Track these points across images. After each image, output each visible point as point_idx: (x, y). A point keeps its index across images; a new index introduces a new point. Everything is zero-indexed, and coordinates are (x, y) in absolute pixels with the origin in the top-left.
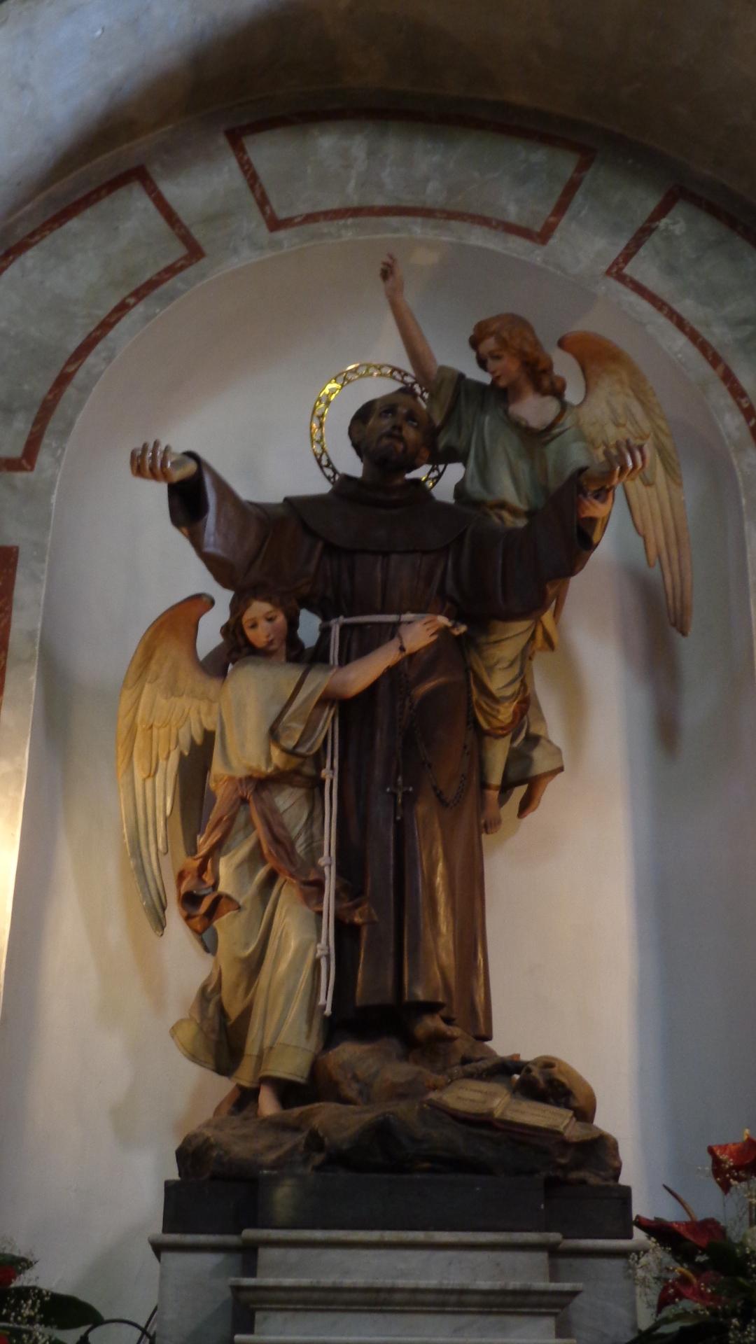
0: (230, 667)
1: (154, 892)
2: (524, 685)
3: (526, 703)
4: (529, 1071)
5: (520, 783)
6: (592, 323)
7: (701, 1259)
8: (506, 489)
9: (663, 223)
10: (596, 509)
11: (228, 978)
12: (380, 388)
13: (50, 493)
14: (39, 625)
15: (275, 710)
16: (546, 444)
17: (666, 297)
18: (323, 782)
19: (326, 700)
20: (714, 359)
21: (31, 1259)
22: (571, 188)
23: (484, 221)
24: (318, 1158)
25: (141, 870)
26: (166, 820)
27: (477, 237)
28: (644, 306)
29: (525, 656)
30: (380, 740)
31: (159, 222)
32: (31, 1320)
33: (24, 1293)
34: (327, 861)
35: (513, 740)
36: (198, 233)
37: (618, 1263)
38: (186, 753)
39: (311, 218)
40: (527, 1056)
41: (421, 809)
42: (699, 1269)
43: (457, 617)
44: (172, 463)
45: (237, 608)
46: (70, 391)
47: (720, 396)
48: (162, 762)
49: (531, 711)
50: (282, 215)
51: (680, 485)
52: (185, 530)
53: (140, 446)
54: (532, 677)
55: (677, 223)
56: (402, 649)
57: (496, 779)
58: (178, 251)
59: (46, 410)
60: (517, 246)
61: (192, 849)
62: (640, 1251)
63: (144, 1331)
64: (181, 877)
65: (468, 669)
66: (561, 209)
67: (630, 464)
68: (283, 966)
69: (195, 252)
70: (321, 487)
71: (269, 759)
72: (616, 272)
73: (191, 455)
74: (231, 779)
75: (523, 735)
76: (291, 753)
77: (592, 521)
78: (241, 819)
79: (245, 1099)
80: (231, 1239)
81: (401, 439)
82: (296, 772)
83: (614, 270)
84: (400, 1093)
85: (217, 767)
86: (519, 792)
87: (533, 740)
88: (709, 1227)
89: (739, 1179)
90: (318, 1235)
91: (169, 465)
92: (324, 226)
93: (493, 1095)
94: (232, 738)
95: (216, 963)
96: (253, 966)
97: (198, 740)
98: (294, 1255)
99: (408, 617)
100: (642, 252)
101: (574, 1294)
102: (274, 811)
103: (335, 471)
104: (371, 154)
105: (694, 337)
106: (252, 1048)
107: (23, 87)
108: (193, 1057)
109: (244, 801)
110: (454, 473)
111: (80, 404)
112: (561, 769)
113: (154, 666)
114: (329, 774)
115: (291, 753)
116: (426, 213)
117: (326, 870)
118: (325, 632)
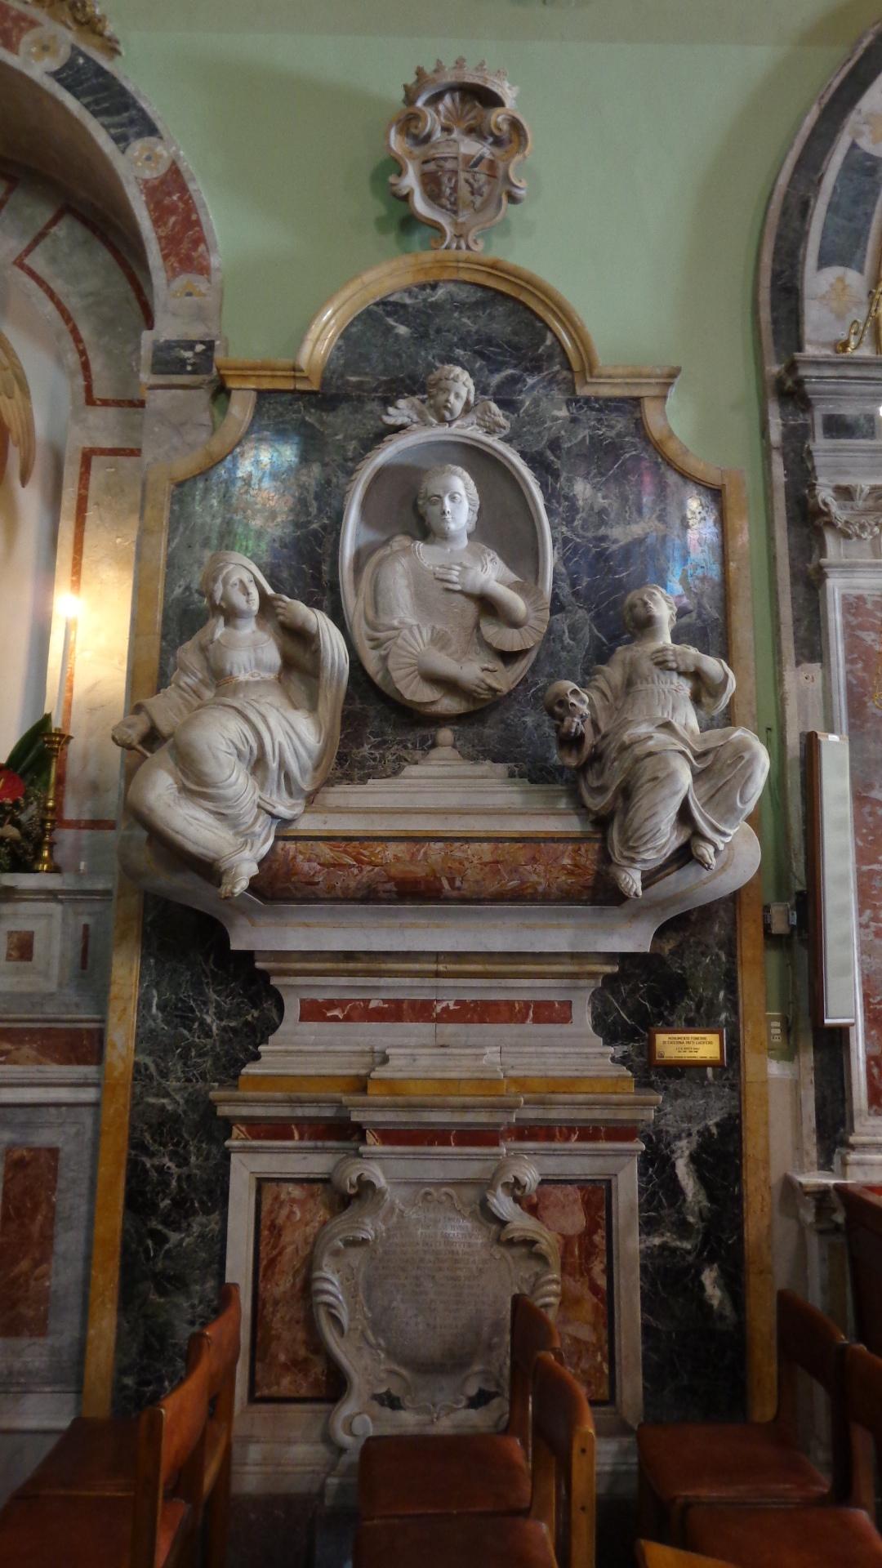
9: (54, 230)
28: (32, 284)
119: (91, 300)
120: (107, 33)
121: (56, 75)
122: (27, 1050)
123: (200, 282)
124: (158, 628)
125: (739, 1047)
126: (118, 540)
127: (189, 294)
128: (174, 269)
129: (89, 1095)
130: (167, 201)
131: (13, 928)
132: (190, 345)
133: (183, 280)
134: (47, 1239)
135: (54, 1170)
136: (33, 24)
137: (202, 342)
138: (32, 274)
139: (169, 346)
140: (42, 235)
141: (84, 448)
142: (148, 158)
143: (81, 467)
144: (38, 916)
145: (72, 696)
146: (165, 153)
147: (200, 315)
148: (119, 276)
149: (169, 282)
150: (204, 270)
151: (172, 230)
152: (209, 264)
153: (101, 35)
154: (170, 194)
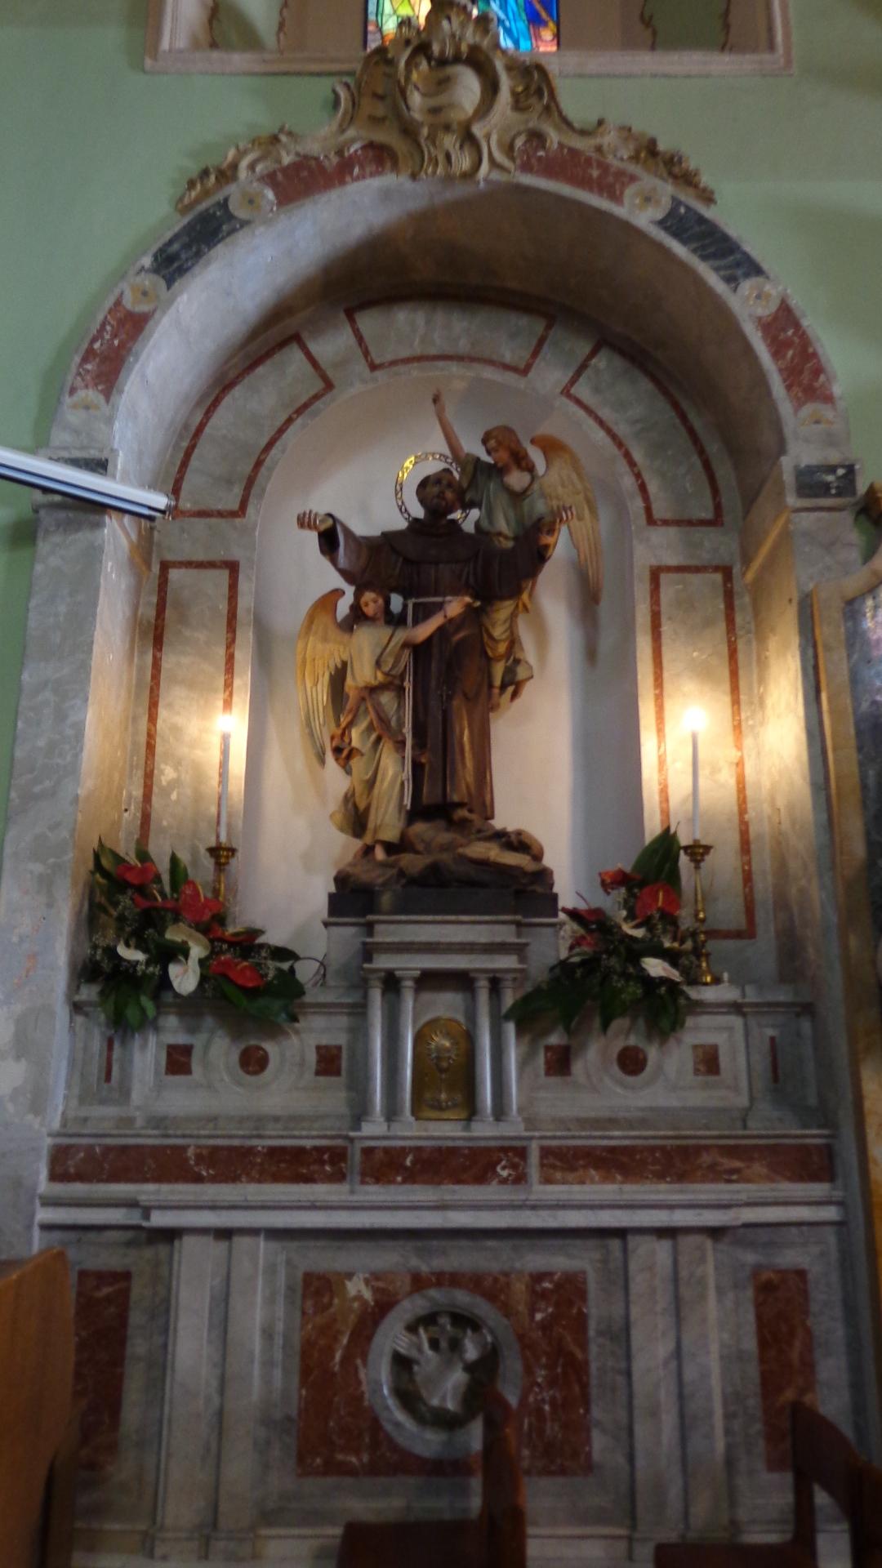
0: (355, 627)
1: (318, 745)
2: (512, 633)
3: (513, 642)
4: (509, 837)
5: (511, 684)
6: (546, 429)
7: (594, 926)
8: (502, 524)
9: (594, 361)
10: (547, 540)
11: (359, 790)
12: (433, 467)
13: (254, 529)
14: (252, 605)
15: (379, 651)
16: (524, 499)
17: (593, 407)
18: (404, 689)
19: (405, 645)
20: (620, 444)
21: (264, 930)
22: (541, 342)
23: (491, 362)
24: (403, 881)
25: (311, 734)
26: (324, 708)
27: (489, 373)
28: (581, 413)
29: (513, 617)
30: (434, 666)
31: (308, 367)
32: (265, 958)
33: (262, 946)
34: (408, 730)
35: (507, 661)
36: (330, 373)
37: (549, 930)
38: (333, 673)
39: (393, 363)
40: (510, 828)
41: (457, 703)
42: (590, 931)
43: (476, 597)
44: (320, 521)
45: (358, 595)
46: (263, 470)
47: (622, 466)
48: (320, 679)
49: (516, 645)
50: (377, 361)
51: (598, 520)
52: (328, 557)
53: (302, 512)
54: (517, 626)
55: (601, 362)
56: (445, 616)
57: (497, 682)
58: (319, 385)
59: (250, 482)
60: (510, 378)
61: (338, 725)
62: (562, 924)
63: (322, 963)
64: (332, 738)
65: (481, 625)
66: (535, 353)
67: (565, 518)
68: (386, 784)
69: (329, 385)
70: (401, 524)
71: (376, 678)
72: (566, 392)
73: (330, 515)
74: (357, 688)
75: (512, 658)
76: (387, 674)
77: (547, 547)
78: (362, 708)
79: (368, 850)
80: (361, 920)
81: (444, 498)
82: (391, 683)
83: (565, 391)
84: (444, 848)
85: (349, 682)
86: (511, 689)
87: (517, 662)
88: (598, 912)
89: (613, 889)
90: (403, 918)
91: (318, 522)
92: (402, 368)
93: (489, 849)
94: (356, 666)
95: (352, 783)
96: (371, 784)
97: (339, 666)
98: (392, 927)
99: (448, 598)
100: (581, 379)
101: (526, 945)
102: (379, 704)
103: (409, 515)
104: (428, 322)
105: (609, 432)
106: (371, 825)
107: (228, 294)
108: (342, 830)
109: (363, 699)
110: (475, 514)
111: (269, 478)
112: (532, 677)
113: (314, 627)
114: (408, 685)
115: (387, 674)
116: (459, 358)
117: (407, 736)
118: (405, 606)
119: (639, 426)
120: (702, 185)
121: (662, 223)
122: (758, 1168)
123: (827, 412)
124: (853, 742)
125: (419, 1149)
126: (695, 654)
127: (817, 422)
128: (798, 399)
129: (830, 1213)
130: (782, 336)
131: (697, 1042)
132: (832, 469)
133: (808, 409)
134: (808, 1366)
135: (805, 1293)
136: (633, 178)
137: (843, 466)
138: (579, 402)
139: (810, 470)
140: (583, 367)
141: (651, 567)
142: (758, 297)
143: (651, 584)
144: (719, 1029)
145: (668, 806)
146: (774, 293)
147: (831, 440)
148: (662, 404)
149: (796, 411)
150: (829, 399)
151: (792, 362)
152: (832, 394)
153: (696, 186)
154: (784, 330)
